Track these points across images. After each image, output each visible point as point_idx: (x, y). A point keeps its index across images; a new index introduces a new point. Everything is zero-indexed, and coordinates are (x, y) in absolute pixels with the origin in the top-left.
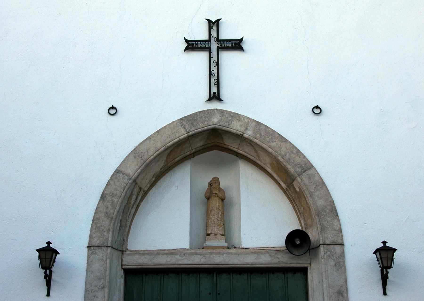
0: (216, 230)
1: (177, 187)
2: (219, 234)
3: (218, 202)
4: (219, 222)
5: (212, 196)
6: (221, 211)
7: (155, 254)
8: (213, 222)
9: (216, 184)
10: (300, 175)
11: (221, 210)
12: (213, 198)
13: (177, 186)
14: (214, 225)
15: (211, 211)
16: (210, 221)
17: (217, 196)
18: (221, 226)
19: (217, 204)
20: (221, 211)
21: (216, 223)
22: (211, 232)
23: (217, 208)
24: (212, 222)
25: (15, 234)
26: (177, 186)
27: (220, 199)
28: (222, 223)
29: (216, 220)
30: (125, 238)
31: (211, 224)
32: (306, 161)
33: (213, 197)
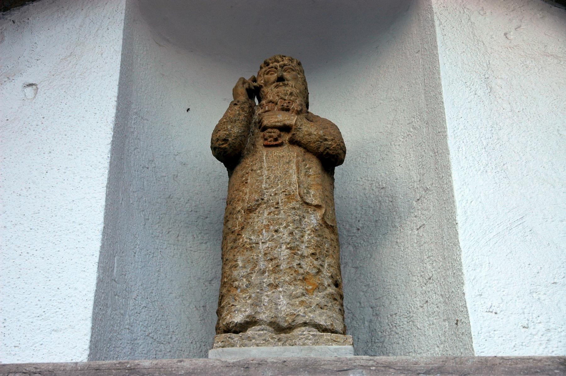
0: (283, 301)
1: (29, 90)
2: (305, 324)
3: (294, 167)
4: (308, 265)
5: (261, 142)
6: (319, 214)
7: (129, 303)
8: (262, 265)
9: (285, 85)
10: (353, 338)
11: (318, 207)
12: (264, 152)
13: (31, 85)
14: (267, 279)
15: (250, 210)
16: (240, 264)
17: (293, 142)
18: (318, 288)
19: (294, 178)
20: (319, 214)
21: (283, 266)
22: (249, 311)
23: (289, 197)
24: (256, 264)
25: (57, 75)
26: (31, 85)
27: (308, 156)
28: (326, 273)
29: (285, 252)
30: (332, 124)
31: (248, 276)
32: (286, 246)
33: (266, 146)
